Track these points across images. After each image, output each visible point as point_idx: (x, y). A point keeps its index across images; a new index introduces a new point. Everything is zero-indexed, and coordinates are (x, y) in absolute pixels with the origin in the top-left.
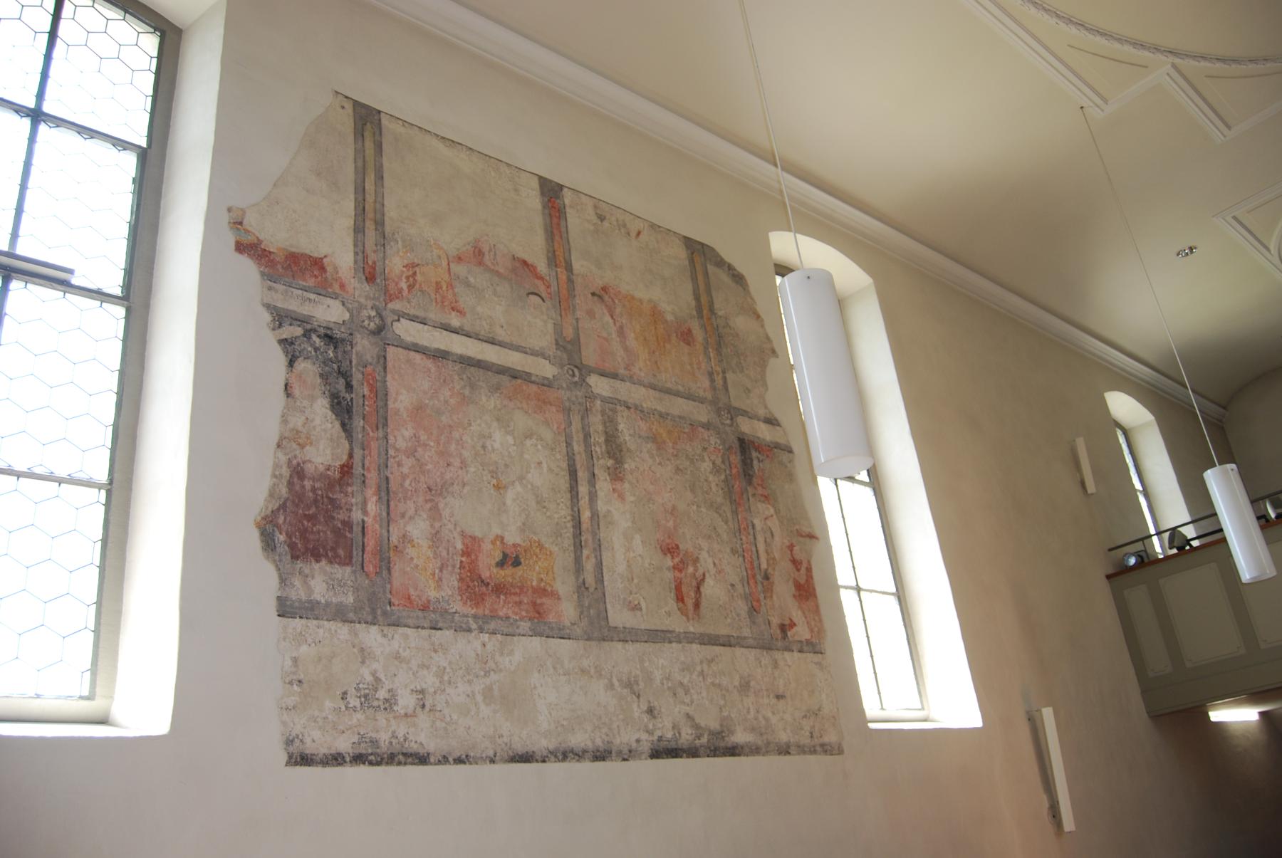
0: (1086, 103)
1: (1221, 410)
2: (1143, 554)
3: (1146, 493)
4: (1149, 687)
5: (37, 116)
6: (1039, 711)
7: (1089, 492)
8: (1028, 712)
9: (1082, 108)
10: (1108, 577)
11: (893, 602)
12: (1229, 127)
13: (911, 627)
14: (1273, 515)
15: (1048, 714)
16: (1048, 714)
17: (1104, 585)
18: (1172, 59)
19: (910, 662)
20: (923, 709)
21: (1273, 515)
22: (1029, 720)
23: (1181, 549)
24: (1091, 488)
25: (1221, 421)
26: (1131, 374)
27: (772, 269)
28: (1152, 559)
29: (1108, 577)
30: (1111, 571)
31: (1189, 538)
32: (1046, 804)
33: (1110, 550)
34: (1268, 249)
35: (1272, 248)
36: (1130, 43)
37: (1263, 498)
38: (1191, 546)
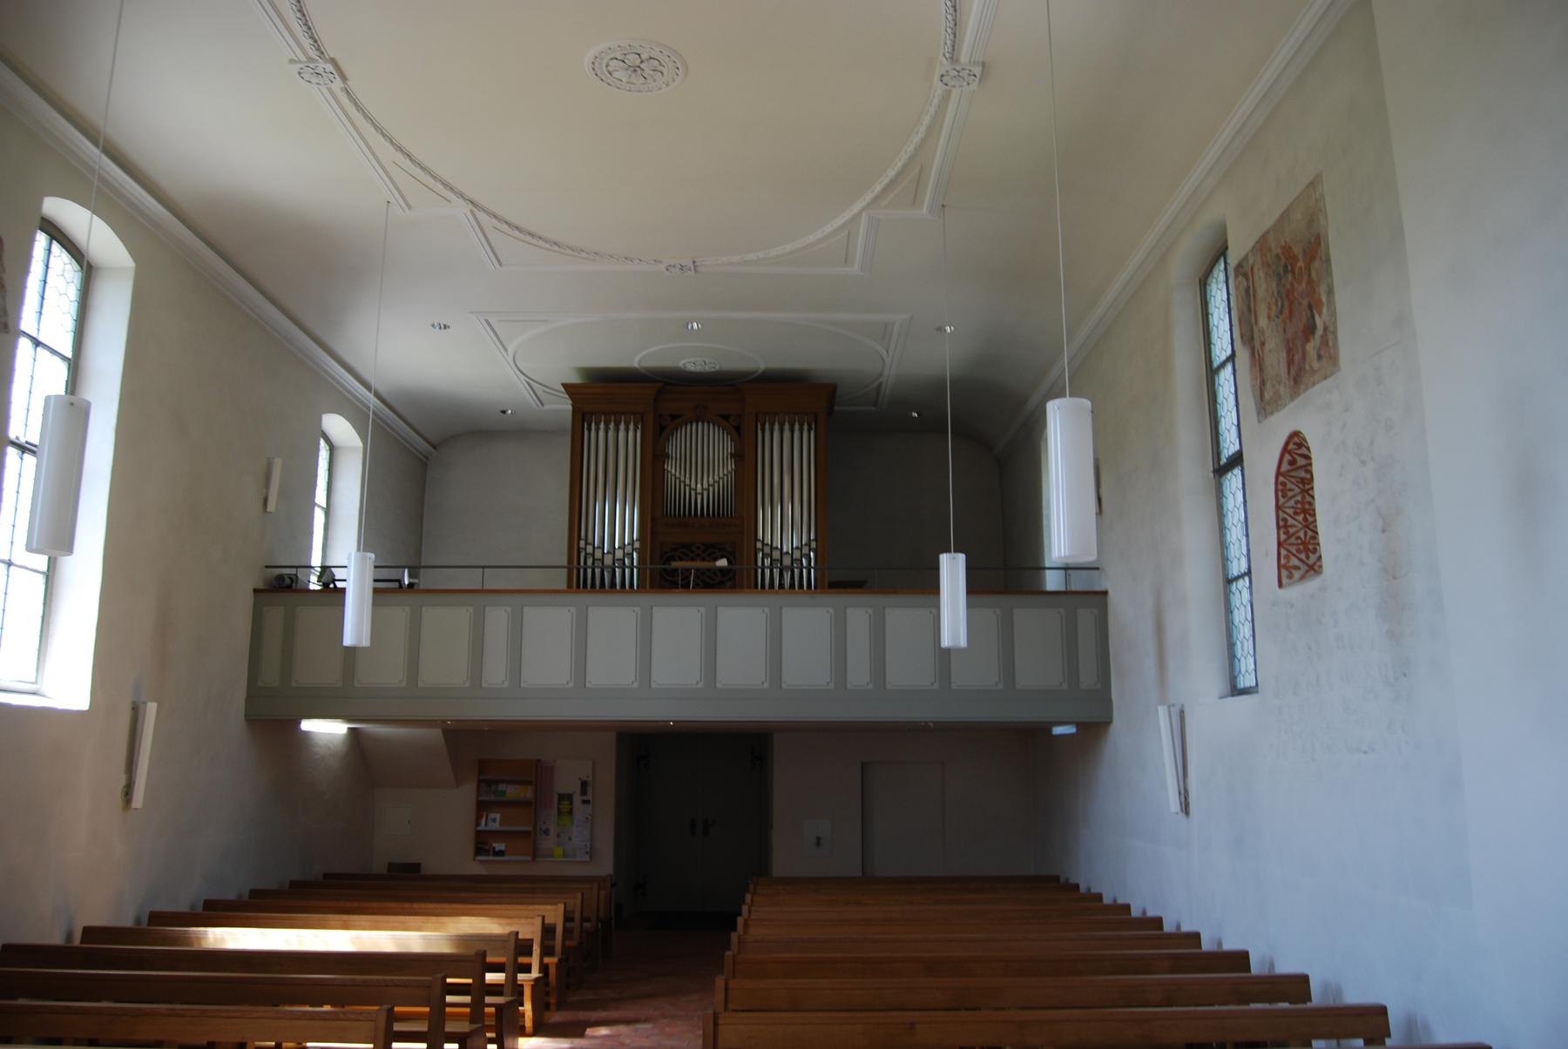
0: (392, 200)
1: (432, 450)
2: (294, 577)
3: (328, 511)
4: (255, 693)
5: (9, 564)
6: (145, 703)
7: (268, 510)
8: (134, 703)
9: (389, 202)
10: (256, 591)
11: (41, 579)
12: (500, 264)
13: (50, 607)
14: (407, 582)
15: (152, 708)
16: (152, 708)
17: (250, 596)
18: (471, 206)
19: (38, 639)
20: (36, 683)
21: (407, 582)
22: (133, 709)
23: (326, 585)
24: (271, 507)
25: (427, 458)
26: (358, 399)
27: (37, 222)
28: (300, 586)
29: (256, 591)
30: (261, 586)
31: (336, 578)
32: (123, 782)
33: (267, 567)
34: (506, 350)
35: (510, 350)
36: (443, 183)
37: (404, 567)
38: (335, 585)
